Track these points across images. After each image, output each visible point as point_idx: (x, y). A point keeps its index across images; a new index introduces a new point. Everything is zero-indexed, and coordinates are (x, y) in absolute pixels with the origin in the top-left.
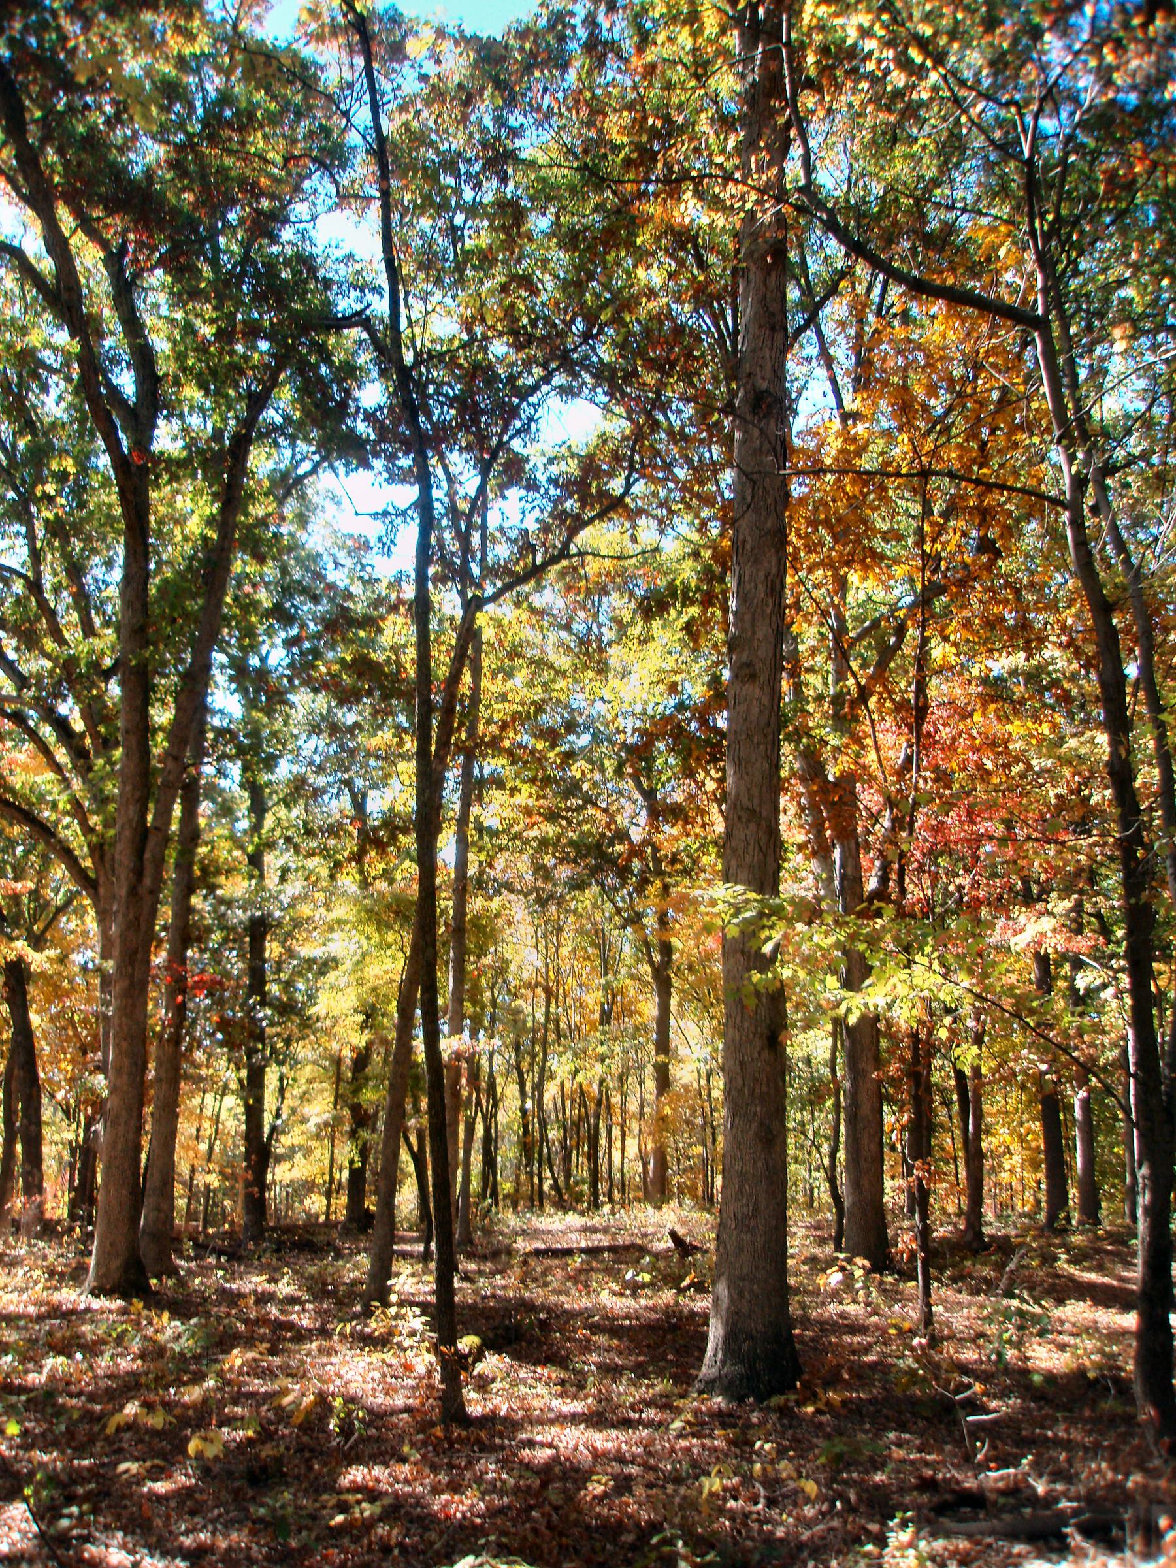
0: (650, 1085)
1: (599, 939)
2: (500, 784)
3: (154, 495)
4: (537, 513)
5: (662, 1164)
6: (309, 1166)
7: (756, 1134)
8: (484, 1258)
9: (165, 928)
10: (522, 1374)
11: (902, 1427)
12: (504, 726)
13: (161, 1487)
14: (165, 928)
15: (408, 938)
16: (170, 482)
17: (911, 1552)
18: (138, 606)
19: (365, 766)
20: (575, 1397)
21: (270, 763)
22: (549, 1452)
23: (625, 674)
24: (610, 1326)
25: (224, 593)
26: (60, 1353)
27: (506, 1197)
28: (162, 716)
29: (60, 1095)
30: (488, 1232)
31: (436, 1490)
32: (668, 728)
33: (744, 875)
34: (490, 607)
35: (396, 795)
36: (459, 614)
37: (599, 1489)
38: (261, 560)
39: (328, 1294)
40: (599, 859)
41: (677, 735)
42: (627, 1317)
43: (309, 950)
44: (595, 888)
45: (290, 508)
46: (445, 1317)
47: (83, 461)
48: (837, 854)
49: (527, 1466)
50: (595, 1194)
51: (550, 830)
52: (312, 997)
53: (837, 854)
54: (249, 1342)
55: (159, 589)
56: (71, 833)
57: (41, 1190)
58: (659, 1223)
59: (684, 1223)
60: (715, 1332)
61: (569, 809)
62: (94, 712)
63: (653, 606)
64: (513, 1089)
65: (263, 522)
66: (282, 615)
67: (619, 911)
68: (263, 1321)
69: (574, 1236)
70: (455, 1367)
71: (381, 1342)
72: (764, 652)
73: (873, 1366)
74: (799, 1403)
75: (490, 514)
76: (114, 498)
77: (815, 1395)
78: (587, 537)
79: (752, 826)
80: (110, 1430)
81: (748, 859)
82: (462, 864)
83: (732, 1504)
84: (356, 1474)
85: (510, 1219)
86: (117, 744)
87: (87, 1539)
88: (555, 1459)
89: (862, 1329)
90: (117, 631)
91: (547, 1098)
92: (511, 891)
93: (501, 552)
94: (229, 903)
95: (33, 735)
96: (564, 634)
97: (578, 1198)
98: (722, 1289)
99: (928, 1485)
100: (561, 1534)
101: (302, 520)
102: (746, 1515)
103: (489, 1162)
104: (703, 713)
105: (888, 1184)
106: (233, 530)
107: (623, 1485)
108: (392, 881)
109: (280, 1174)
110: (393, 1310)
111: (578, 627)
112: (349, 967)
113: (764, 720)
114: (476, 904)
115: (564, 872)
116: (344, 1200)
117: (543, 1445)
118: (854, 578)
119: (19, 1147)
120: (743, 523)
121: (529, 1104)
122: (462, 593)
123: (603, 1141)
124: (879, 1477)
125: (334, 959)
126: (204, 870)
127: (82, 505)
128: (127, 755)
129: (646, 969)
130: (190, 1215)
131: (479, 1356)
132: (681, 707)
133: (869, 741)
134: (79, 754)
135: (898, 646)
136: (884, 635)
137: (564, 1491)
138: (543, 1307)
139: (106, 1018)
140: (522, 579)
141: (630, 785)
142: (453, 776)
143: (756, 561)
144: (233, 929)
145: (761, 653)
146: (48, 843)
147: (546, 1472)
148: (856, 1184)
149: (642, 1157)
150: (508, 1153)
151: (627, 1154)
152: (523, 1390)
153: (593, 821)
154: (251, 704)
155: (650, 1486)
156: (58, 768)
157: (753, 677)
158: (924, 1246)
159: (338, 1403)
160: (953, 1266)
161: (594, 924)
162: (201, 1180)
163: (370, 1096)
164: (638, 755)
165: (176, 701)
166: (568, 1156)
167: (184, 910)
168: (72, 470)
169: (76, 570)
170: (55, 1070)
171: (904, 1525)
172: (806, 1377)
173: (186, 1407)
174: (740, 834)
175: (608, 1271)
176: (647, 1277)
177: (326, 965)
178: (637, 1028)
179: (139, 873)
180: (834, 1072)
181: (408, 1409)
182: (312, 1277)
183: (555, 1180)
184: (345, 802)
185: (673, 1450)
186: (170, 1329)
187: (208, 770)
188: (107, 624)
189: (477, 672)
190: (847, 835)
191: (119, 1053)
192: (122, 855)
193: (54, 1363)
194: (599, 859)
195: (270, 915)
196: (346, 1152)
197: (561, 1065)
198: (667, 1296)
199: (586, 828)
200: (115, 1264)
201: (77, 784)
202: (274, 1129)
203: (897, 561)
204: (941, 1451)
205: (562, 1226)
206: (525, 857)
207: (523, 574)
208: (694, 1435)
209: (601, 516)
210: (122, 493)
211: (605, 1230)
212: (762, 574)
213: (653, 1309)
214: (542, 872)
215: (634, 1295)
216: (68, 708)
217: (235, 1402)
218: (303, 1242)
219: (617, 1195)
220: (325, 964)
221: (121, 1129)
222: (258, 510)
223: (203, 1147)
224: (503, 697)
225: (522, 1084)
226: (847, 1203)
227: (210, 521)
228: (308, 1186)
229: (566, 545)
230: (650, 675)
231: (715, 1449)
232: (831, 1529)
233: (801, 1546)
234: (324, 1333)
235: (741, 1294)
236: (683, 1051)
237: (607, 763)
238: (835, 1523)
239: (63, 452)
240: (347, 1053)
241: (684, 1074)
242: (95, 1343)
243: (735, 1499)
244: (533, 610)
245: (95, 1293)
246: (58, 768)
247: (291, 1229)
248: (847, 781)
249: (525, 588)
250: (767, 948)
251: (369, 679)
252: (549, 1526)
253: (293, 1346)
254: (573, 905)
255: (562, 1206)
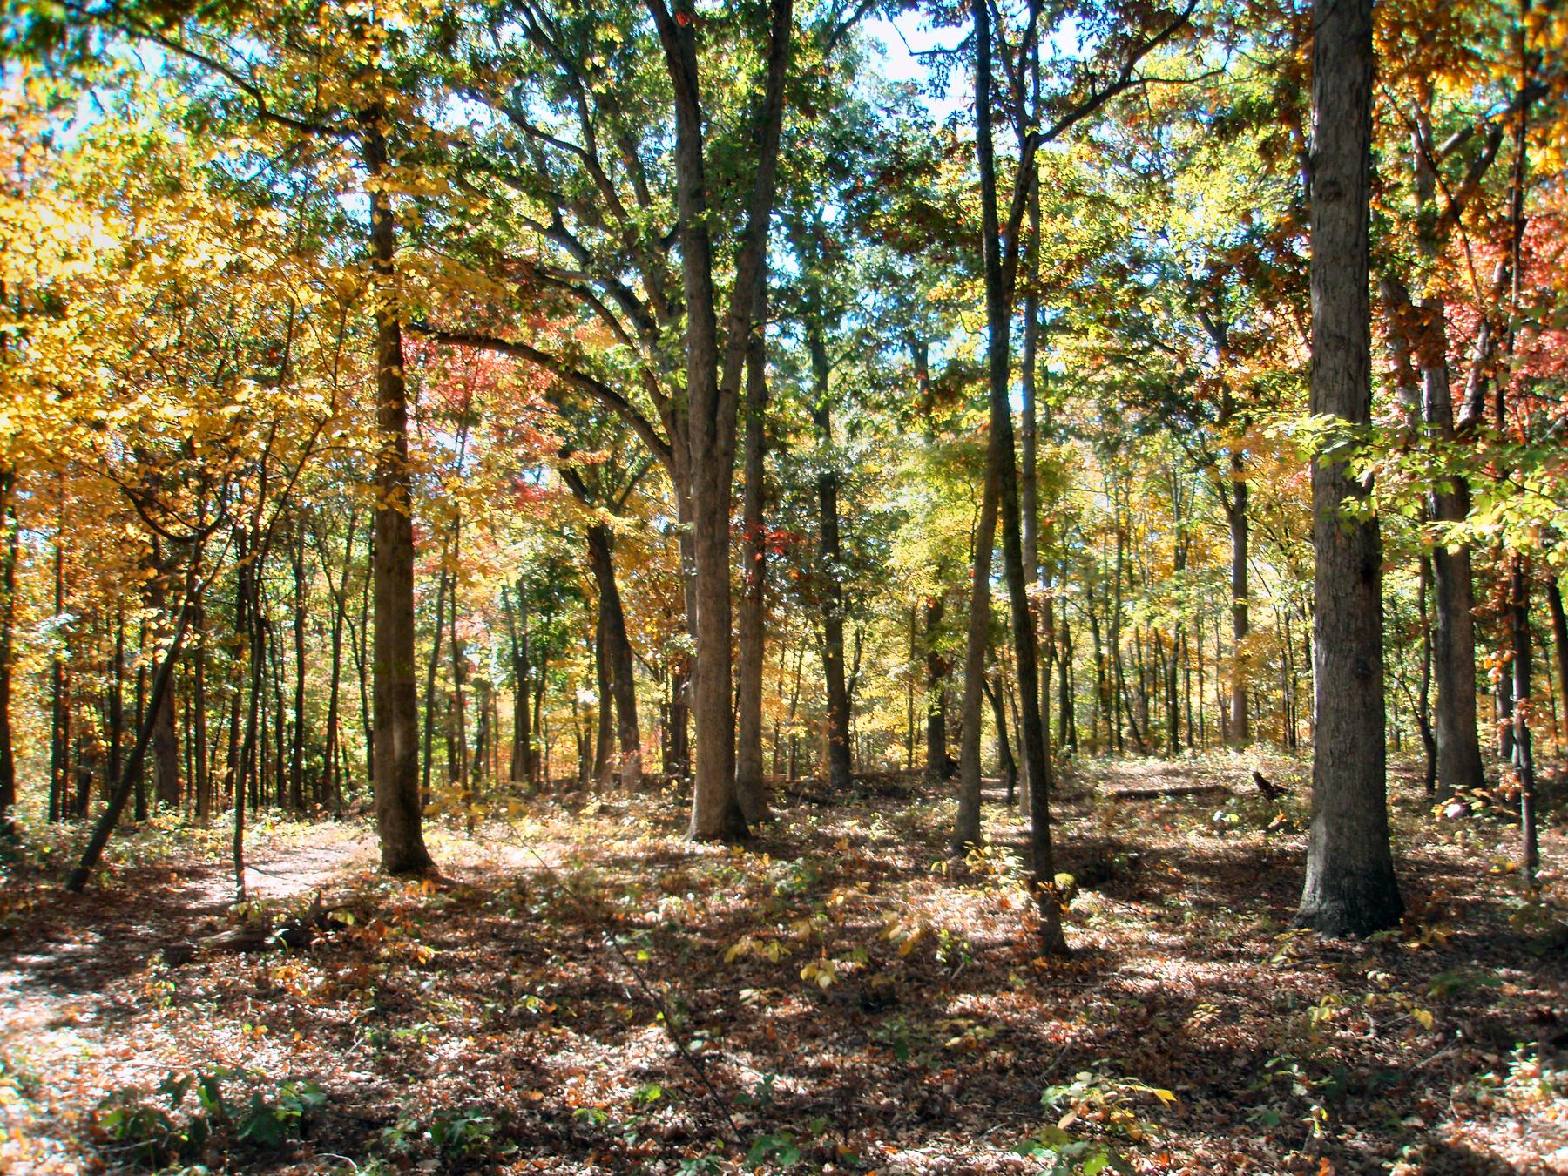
0: (1228, 629)
1: (1170, 483)
2: (1065, 328)
3: (700, 58)
4: (1094, 40)
5: (1242, 709)
6: (890, 716)
7: (1352, 671)
8: (1068, 801)
9: (739, 489)
10: (1117, 910)
11: (1514, 964)
12: (1069, 266)
13: (781, 1012)
14: (739, 489)
15: (980, 489)
16: (716, 42)
17: (1536, 1081)
18: (693, 169)
19: (924, 318)
20: (1172, 932)
21: (833, 318)
22: (1152, 983)
23: (1190, 207)
24: (1202, 865)
25: (778, 151)
26: (672, 893)
27: (1084, 743)
28: (725, 277)
29: (649, 657)
30: (1069, 777)
31: (1044, 1017)
32: (1245, 261)
33: (1334, 404)
34: (1045, 146)
35: (966, 340)
36: (1017, 154)
37: (1207, 1018)
38: (811, 113)
39: (920, 837)
40: (1167, 401)
41: (1253, 264)
42: (1216, 856)
43: (876, 506)
44: (1166, 432)
45: (837, 58)
46: (1040, 855)
47: (626, 27)
48: (1424, 386)
49: (1131, 994)
50: (1175, 738)
51: (1118, 374)
52: (886, 554)
53: (1424, 386)
54: (849, 881)
55: (711, 152)
56: (640, 398)
57: (638, 747)
58: (1243, 766)
59: (1268, 766)
60: (1313, 870)
61: (1135, 351)
62: (656, 280)
63: (1227, 127)
64: (1087, 637)
65: (811, 75)
66: (835, 169)
67: (1191, 454)
68: (860, 862)
69: (1156, 780)
70: (1053, 905)
71: (977, 880)
72: (1350, 168)
73: (1475, 904)
74: (1403, 939)
75: (1041, 48)
76: (659, 65)
77: (1419, 931)
78: (1144, 65)
79: (1340, 353)
80: (729, 958)
81: (1337, 388)
82: (1029, 412)
83: (1340, 1033)
84: (966, 1001)
85: (1092, 765)
86: (682, 309)
87: (720, 1058)
88: (1159, 989)
89: (1462, 870)
90: (675, 199)
91: (1122, 645)
92: (1080, 437)
93: (1054, 85)
94: (800, 461)
95: (598, 306)
96: (1123, 171)
97: (1158, 743)
98: (1320, 827)
99: (1545, 1019)
100: (1172, 1058)
101: (849, 70)
102: (1358, 1044)
103: (1067, 711)
104: (1277, 241)
105: (1480, 726)
106: (783, 87)
107: (1231, 1014)
108: (958, 432)
109: (861, 725)
110: (988, 850)
111: (1140, 161)
112: (923, 519)
113: (1351, 240)
114: (1046, 451)
115: (1132, 416)
116: (924, 749)
117: (1144, 976)
118: (1442, 83)
119: (614, 709)
120: (1324, 30)
121: (1104, 651)
122: (1019, 132)
123: (1180, 687)
124: (1492, 1010)
125: (905, 513)
126: (774, 430)
127: (630, 74)
128: (692, 320)
129: (1221, 512)
130: (779, 767)
131: (1073, 894)
132: (1252, 234)
133: (1463, 261)
134: (645, 323)
135: (1490, 159)
136: (1476, 145)
137: (1171, 1018)
138: (1131, 848)
139: (688, 577)
140: (1081, 112)
141: (1198, 323)
142: (1016, 323)
143: (1339, 71)
144: (802, 489)
145: (1346, 170)
146: (621, 413)
147: (1153, 1001)
148: (1451, 725)
149: (1222, 703)
150: (1084, 699)
151: (1206, 697)
152: (1120, 924)
153: (1161, 364)
154: (808, 262)
155: (1257, 1015)
156: (626, 339)
157: (1338, 195)
158: (1528, 787)
159: (943, 935)
160: (1557, 807)
161: (1165, 468)
162: (786, 732)
163: (947, 644)
164: (1206, 294)
165: (736, 264)
166: (1143, 703)
167: (757, 470)
168: (618, 39)
169: (628, 142)
170: (642, 632)
171: (1526, 1056)
172: (1409, 913)
173: (796, 940)
174: (1329, 362)
175: (1191, 812)
176: (1235, 818)
177: (894, 521)
178: (1213, 572)
179: (712, 435)
180: (1423, 610)
181: (1008, 943)
182: (901, 821)
183: (1133, 723)
184: (908, 357)
185: (1276, 983)
186: (778, 872)
187: (772, 330)
188: (664, 193)
189: (1036, 216)
190: (1434, 360)
191: (706, 611)
192: (695, 417)
193: (670, 903)
194: (1167, 401)
195: (840, 473)
196: (925, 703)
197: (1136, 611)
198: (1256, 837)
199: (1153, 369)
200: (715, 812)
201: (645, 353)
202: (853, 682)
203: (1491, 62)
204: (1555, 987)
205: (1143, 770)
206: (1092, 403)
207: (1076, 111)
208: (1296, 968)
209: (1162, 39)
210: (670, 59)
211: (1187, 774)
212: (1346, 84)
213: (1243, 849)
214: (1111, 415)
215: (1222, 835)
216: (631, 279)
217: (842, 937)
218: (889, 789)
219: (1196, 740)
220: (895, 519)
221: (713, 684)
222: (803, 63)
223: (786, 702)
224: (1063, 238)
225: (1096, 631)
226: (1440, 743)
227: (757, 79)
228: (888, 737)
229: (1127, 71)
230: (1216, 202)
231: (1320, 982)
232: (1446, 1059)
233: (1417, 1074)
234: (919, 872)
235: (1339, 829)
236: (1261, 594)
237: (1174, 301)
238: (1451, 1053)
239: (607, 22)
240: (923, 602)
241: (1262, 618)
242: (704, 884)
243: (1345, 1028)
244: (1091, 142)
245: (699, 838)
246: (626, 339)
247: (874, 777)
248: (1433, 305)
249: (1086, 121)
250: (1362, 479)
251: (930, 227)
252: (1160, 1051)
253: (889, 885)
254: (1142, 450)
255: (1143, 751)
